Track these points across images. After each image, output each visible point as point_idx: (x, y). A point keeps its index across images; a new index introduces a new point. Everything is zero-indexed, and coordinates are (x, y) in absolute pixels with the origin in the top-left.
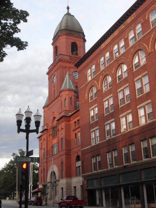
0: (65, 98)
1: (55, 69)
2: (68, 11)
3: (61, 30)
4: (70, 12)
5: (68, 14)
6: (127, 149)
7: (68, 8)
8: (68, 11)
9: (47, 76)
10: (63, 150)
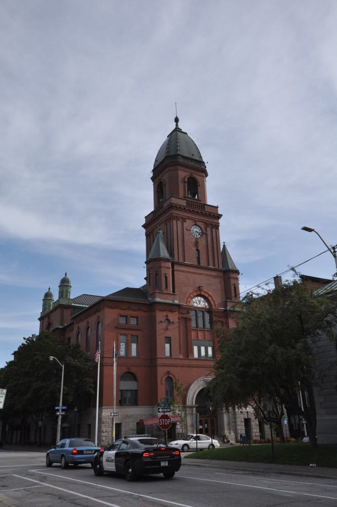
0: (157, 272)
1: (162, 218)
2: (177, 125)
3: (170, 156)
4: (180, 126)
5: (177, 130)
6: (205, 387)
7: (177, 120)
8: (177, 125)
9: (144, 230)
10: (234, 304)
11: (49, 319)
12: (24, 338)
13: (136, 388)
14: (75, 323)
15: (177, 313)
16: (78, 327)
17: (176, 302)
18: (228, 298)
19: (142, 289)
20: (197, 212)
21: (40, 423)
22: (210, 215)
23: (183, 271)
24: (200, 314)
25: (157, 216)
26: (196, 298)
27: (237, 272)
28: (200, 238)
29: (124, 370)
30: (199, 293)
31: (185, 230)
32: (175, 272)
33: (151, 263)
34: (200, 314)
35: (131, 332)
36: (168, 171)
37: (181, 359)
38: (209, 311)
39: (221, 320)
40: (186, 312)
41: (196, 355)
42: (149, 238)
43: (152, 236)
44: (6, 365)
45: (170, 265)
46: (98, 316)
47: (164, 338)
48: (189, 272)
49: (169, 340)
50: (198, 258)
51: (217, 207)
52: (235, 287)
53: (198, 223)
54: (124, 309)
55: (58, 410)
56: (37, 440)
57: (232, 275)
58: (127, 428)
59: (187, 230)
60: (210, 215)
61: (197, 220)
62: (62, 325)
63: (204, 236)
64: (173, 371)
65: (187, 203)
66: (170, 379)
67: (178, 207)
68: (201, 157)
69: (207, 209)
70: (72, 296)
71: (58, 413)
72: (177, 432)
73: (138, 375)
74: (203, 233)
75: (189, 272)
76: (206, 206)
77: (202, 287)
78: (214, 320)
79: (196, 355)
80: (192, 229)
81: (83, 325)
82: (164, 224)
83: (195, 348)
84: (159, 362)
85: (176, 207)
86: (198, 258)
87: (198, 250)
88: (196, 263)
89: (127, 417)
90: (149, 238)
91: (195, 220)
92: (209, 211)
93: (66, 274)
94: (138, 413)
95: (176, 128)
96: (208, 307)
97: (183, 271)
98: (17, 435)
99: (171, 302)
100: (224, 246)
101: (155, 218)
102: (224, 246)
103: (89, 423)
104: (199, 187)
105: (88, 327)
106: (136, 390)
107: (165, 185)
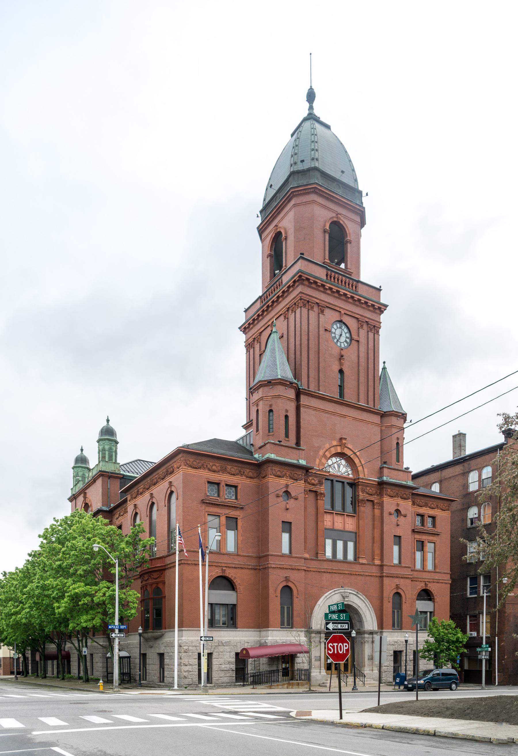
2: (311, 108)
4: (317, 112)
8: (311, 108)
11: (85, 497)
12: (40, 536)
13: (235, 602)
14: (128, 499)
15: (303, 482)
16: (135, 505)
17: (303, 462)
18: (385, 463)
19: (241, 442)
20: (345, 295)
21: (84, 649)
22: (366, 303)
23: (315, 409)
24: (338, 487)
25: (270, 303)
26: (334, 459)
27: (403, 416)
28: (346, 348)
29: (218, 572)
30: (339, 451)
31: (322, 330)
32: (302, 410)
33: (261, 390)
34: (338, 487)
35: (227, 511)
36: (295, 205)
37: (305, 559)
38: (353, 485)
39: (371, 498)
40: (317, 482)
41: (329, 553)
42: (252, 351)
43: (257, 346)
44: (13, 571)
45: (291, 394)
46: (171, 482)
47: (281, 522)
48: (324, 411)
49: (287, 526)
50: (341, 387)
51: (379, 290)
52: (398, 444)
53: (347, 319)
54: (214, 471)
55: (113, 631)
56: (82, 674)
57: (394, 421)
58: (222, 661)
59: (326, 330)
60: (366, 303)
61: (343, 312)
62: (107, 506)
63: (354, 343)
64: (294, 576)
65: (327, 275)
66: (287, 590)
67: (312, 279)
68: (356, 180)
69: (362, 290)
70: (122, 459)
71: (113, 635)
72: (296, 668)
73: (237, 582)
74: (351, 339)
75: (324, 411)
76: (360, 285)
77: (345, 439)
78: (361, 498)
79: (329, 553)
80: (333, 330)
81: (142, 501)
82: (282, 318)
83: (329, 543)
84: (272, 562)
85: (308, 279)
86: (341, 387)
87: (341, 371)
88: (336, 396)
89: (221, 644)
90: (252, 351)
91: (340, 312)
92: (365, 295)
93: (108, 421)
94: (238, 639)
95: (310, 114)
96: (351, 476)
97: (315, 409)
98: (53, 665)
99: (295, 462)
100: (384, 368)
101: (265, 308)
102: (384, 368)
103: (162, 652)
104: (349, 245)
105: (153, 504)
106: (234, 605)
107: (286, 239)
